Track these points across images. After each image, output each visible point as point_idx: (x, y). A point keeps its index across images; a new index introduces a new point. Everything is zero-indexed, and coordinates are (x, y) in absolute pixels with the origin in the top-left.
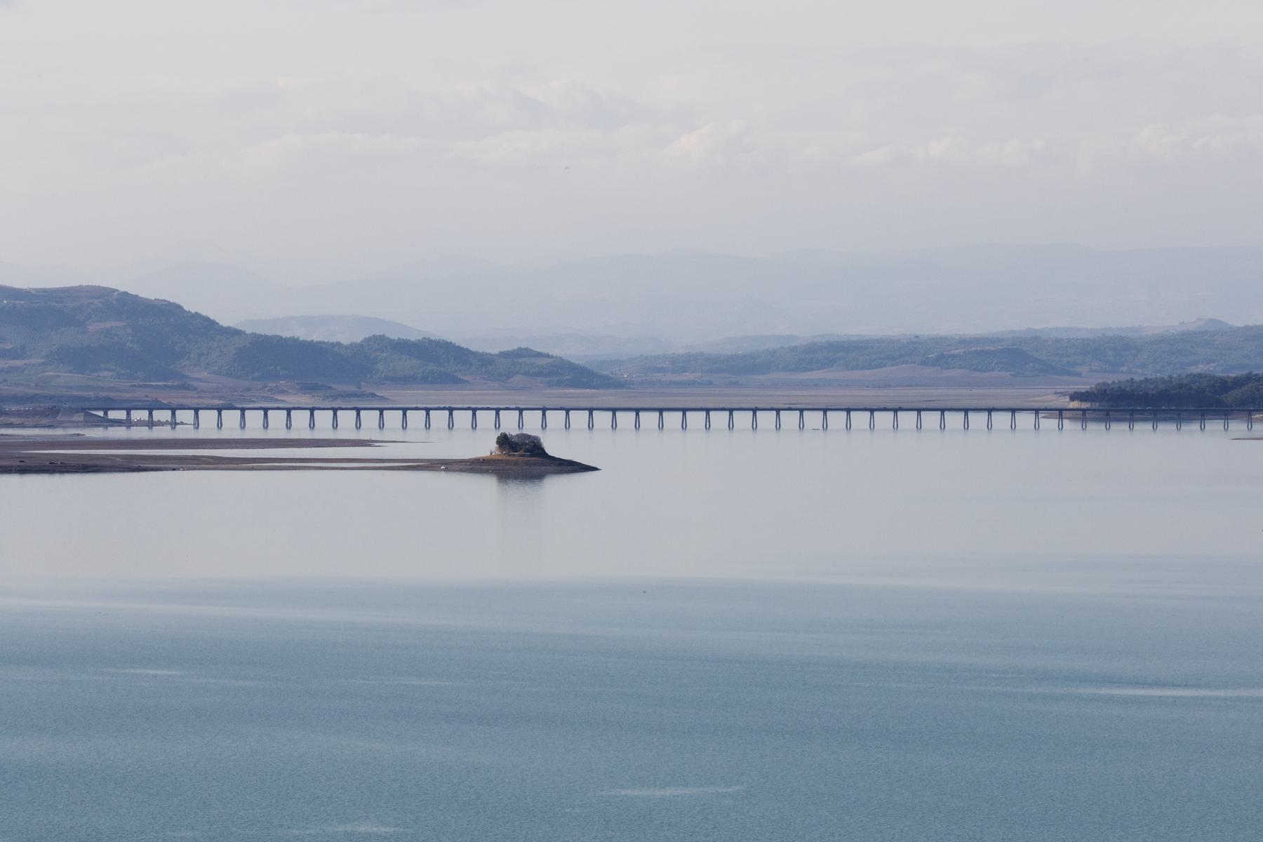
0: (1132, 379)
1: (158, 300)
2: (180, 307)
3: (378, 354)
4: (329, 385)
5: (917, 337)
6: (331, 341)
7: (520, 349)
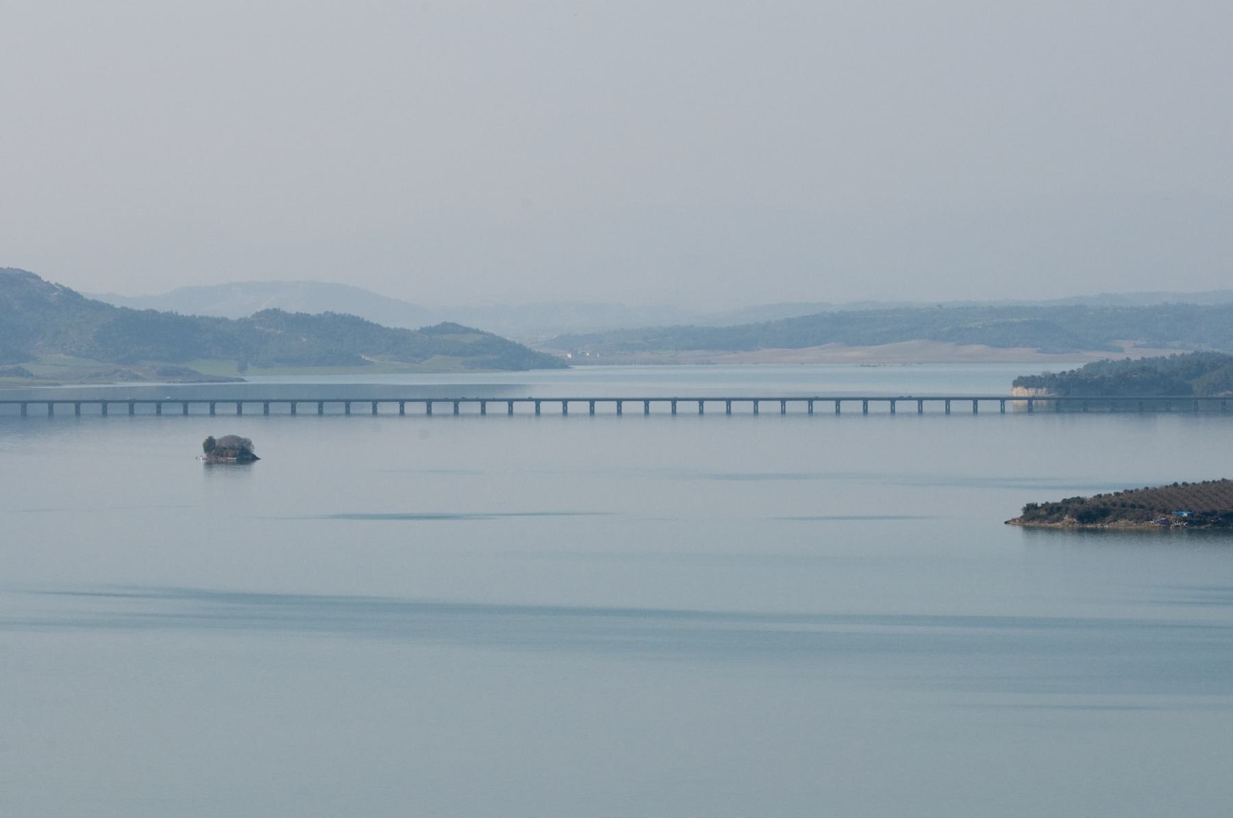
0: (1128, 359)
1: (12, 269)
2: (154, 312)
3: (272, 330)
4: (242, 377)
5: (940, 306)
6: (216, 316)
7: (445, 324)
